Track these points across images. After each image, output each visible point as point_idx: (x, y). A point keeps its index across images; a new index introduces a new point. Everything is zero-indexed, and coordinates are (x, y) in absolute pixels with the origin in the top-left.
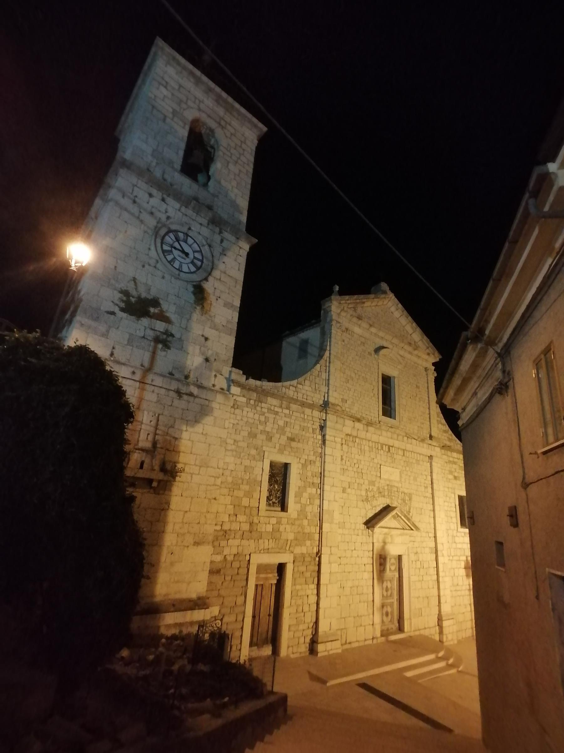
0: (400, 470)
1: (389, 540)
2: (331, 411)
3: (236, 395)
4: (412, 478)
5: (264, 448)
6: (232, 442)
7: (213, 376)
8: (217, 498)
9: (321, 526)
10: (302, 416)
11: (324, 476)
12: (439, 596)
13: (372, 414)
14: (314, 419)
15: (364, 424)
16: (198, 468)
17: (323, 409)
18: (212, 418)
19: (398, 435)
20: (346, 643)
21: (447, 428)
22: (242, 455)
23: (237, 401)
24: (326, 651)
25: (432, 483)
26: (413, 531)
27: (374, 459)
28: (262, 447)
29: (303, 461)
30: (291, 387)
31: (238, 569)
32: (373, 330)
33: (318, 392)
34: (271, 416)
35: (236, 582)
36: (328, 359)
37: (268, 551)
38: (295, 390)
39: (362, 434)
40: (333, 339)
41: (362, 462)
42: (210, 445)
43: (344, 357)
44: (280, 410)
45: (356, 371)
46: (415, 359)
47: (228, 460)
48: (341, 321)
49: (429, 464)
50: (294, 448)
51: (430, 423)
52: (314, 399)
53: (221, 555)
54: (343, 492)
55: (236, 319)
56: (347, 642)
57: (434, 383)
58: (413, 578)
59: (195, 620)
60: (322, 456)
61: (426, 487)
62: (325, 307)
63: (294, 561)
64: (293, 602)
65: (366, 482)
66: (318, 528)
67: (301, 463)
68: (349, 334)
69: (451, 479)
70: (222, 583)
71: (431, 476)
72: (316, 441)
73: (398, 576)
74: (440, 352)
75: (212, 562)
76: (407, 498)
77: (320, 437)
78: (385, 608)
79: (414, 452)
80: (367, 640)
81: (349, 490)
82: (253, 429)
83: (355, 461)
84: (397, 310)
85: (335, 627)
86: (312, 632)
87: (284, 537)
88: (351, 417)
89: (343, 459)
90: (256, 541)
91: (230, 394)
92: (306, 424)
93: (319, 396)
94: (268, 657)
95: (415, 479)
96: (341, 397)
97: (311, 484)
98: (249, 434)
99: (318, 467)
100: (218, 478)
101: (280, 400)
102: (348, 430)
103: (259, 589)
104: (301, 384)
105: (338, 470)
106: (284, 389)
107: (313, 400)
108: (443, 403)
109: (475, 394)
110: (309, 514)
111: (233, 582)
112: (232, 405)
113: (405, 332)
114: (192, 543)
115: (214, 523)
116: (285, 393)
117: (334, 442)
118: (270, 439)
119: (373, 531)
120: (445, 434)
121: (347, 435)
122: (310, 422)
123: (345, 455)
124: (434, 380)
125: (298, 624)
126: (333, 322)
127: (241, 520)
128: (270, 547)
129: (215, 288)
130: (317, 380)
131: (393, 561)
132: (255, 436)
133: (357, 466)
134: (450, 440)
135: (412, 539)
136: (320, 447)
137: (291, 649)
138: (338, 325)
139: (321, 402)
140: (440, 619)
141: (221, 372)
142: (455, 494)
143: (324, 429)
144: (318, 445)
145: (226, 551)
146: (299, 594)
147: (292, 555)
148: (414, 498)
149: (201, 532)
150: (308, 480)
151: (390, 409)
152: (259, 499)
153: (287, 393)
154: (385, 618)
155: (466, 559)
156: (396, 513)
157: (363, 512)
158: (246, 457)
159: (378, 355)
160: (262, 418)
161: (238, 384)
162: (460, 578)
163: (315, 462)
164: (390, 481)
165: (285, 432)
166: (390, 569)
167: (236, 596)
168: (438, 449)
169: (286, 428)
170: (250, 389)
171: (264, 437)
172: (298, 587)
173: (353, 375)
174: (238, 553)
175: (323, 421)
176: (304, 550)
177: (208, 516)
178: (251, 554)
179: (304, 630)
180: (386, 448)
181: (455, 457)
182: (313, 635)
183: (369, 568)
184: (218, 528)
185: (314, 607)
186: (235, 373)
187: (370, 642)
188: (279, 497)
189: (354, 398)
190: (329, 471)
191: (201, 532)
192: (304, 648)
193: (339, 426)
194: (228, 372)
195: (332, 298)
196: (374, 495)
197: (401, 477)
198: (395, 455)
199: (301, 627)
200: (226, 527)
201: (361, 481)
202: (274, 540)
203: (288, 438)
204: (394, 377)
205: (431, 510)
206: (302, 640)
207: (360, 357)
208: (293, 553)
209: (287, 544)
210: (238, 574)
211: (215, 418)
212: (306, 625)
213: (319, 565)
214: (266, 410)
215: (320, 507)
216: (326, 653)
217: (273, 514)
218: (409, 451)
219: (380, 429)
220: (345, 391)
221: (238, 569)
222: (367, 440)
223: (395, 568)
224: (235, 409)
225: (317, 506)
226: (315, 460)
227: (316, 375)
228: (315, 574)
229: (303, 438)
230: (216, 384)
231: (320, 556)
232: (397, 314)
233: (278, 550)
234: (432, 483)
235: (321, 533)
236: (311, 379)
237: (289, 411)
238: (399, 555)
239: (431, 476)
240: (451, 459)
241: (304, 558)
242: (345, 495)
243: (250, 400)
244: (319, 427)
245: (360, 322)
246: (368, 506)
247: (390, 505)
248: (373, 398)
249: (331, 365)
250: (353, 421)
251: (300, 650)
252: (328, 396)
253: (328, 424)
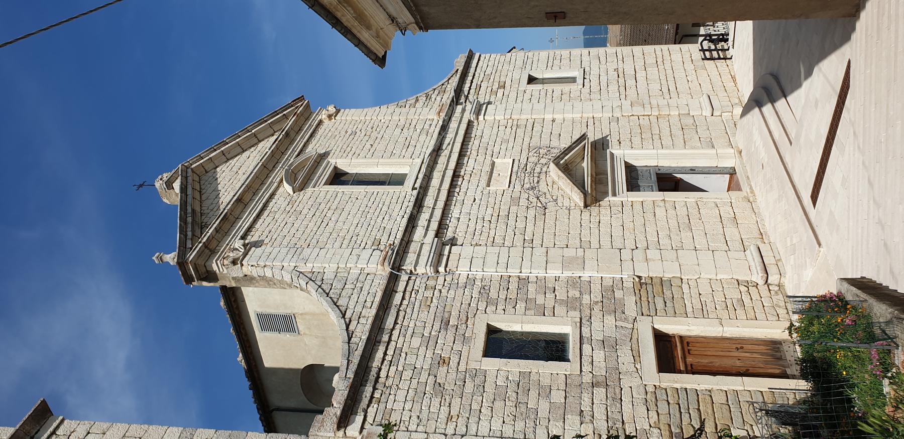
37: (636, 357)
118: (443, 361)
171: (443, 369)
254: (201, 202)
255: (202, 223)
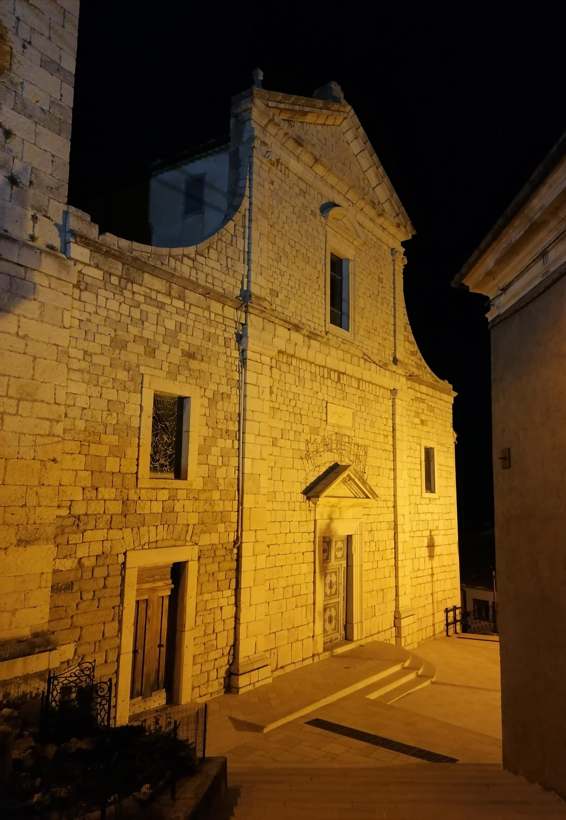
0: (353, 411)
1: (336, 515)
2: (255, 308)
3: (82, 263)
4: (368, 422)
5: (142, 369)
6: (80, 355)
7: (30, 217)
8: (59, 459)
9: (240, 501)
10: (206, 314)
11: (244, 419)
12: (397, 587)
13: (316, 320)
14: (227, 322)
15: (304, 335)
16: (15, 402)
17: (242, 304)
18: (36, 305)
19: (353, 356)
20: (277, 669)
21: (416, 348)
22: (102, 379)
23: (84, 274)
24: (250, 684)
25: (394, 430)
26: (369, 499)
27: (317, 392)
28: (138, 366)
29: (209, 394)
30: (185, 260)
31: (105, 579)
32: (319, 169)
33: (231, 273)
34: (152, 310)
35: (102, 600)
36: (247, 213)
37: (155, 545)
38: (191, 265)
39: (302, 352)
40: (254, 176)
41: (302, 397)
42: (35, 358)
43: (272, 213)
44: (167, 300)
45: (293, 243)
46: (378, 232)
47: (73, 388)
48: (269, 142)
49: (391, 401)
50: (194, 371)
51: (395, 339)
52: (226, 286)
53: (73, 559)
54: (273, 445)
55: (69, 100)
56: (279, 666)
57: (402, 276)
58: (366, 566)
59: (31, 672)
60: (241, 385)
61: (386, 436)
62: (239, 110)
63: (199, 557)
64: (199, 619)
65: (307, 429)
66: (236, 503)
67: (206, 397)
68: (281, 171)
69: (418, 424)
70: (77, 606)
71: (392, 419)
72: (230, 360)
73: (345, 565)
74: (415, 225)
75: (55, 572)
76: (362, 453)
77: (236, 354)
78: (328, 610)
79: (373, 384)
80: (306, 659)
81: (281, 442)
82: (119, 332)
83: (291, 396)
84: (356, 138)
85: (262, 647)
86: (228, 661)
87: (182, 520)
88: (286, 321)
89: (273, 393)
90: (135, 530)
91: (70, 258)
92: (212, 330)
93: (233, 281)
94: (162, 709)
95: (372, 425)
96: (270, 286)
97: (224, 431)
98: (112, 341)
99: (235, 404)
100: (58, 421)
101: (168, 282)
102: (280, 344)
103: (143, 606)
104: (201, 255)
105: (267, 410)
106: (172, 261)
107: (224, 287)
108: (463, 284)
109: (544, 254)
110: (221, 481)
111: (96, 602)
112: (75, 282)
113: (366, 182)
114: (15, 542)
115: (55, 504)
116: (175, 269)
117: (260, 363)
118: (151, 352)
119: (315, 504)
120: (412, 358)
121: (280, 352)
122: (219, 327)
123: (276, 385)
124: (402, 271)
125: (207, 653)
126: (255, 141)
127: (107, 497)
128: (159, 538)
129: (18, 19)
130: (230, 252)
131: (340, 544)
132: (124, 346)
133: (293, 403)
134: (418, 367)
135: (366, 511)
136: (238, 370)
137: (197, 690)
138: (264, 149)
139: (238, 292)
140: (397, 618)
141: (46, 211)
142: (420, 445)
143: (243, 340)
144: (234, 368)
145: (82, 552)
146: (209, 607)
147: (196, 547)
148: (370, 451)
149: (31, 521)
150: (219, 427)
151: (340, 313)
152: (138, 460)
153: (179, 268)
154: (327, 625)
155: (429, 534)
156: (348, 475)
157: (302, 474)
158: (110, 385)
159: (326, 218)
160: (136, 313)
161: (86, 242)
162: (422, 560)
163: (229, 396)
164: (339, 427)
165: (179, 341)
166: (336, 555)
167: (104, 624)
168: (403, 380)
169: (180, 334)
170: (109, 254)
171: (141, 349)
172: (207, 597)
173: (288, 249)
174: (103, 553)
175: (241, 326)
176: (214, 538)
177: (43, 491)
178: (128, 553)
179: (216, 660)
180: (334, 376)
181: (424, 392)
182: (230, 665)
183: (309, 557)
184: (64, 512)
185: (231, 624)
186: (75, 216)
187: (310, 661)
188: (170, 456)
189: (289, 289)
190: (252, 411)
191: (31, 521)
192: (217, 686)
193: (267, 336)
194: (61, 214)
195: (255, 92)
196: (317, 449)
197: (354, 420)
198: (347, 386)
199: (213, 655)
200: (79, 509)
201: (300, 428)
202: (166, 526)
203: (183, 351)
204: (348, 260)
205: (390, 469)
206: (213, 674)
207: (299, 217)
208: (197, 544)
209: (187, 531)
210: (105, 587)
211: (43, 304)
212: (220, 651)
213: (239, 560)
214: (142, 299)
215: (238, 470)
216: (251, 688)
217: (161, 483)
218: (366, 382)
219: (327, 344)
220: (275, 276)
221: (105, 579)
222: (309, 362)
223: (343, 554)
224: (81, 291)
225: (234, 468)
226: (229, 393)
227: (228, 242)
228: (233, 574)
229: (209, 353)
230: (36, 235)
231: (238, 546)
232: (356, 147)
233: (173, 542)
234: (394, 430)
235: (240, 511)
236: (219, 249)
237: (182, 303)
238: (348, 536)
239: (393, 419)
240: (419, 395)
241: (215, 551)
242: (276, 449)
243: (110, 274)
244: (234, 336)
245: (300, 149)
246: (310, 466)
247: (339, 463)
248: (317, 293)
249: (254, 225)
250: (289, 329)
251: (210, 690)
252: (249, 282)
253: (250, 331)
254: (314, 124)
255: (294, 122)
